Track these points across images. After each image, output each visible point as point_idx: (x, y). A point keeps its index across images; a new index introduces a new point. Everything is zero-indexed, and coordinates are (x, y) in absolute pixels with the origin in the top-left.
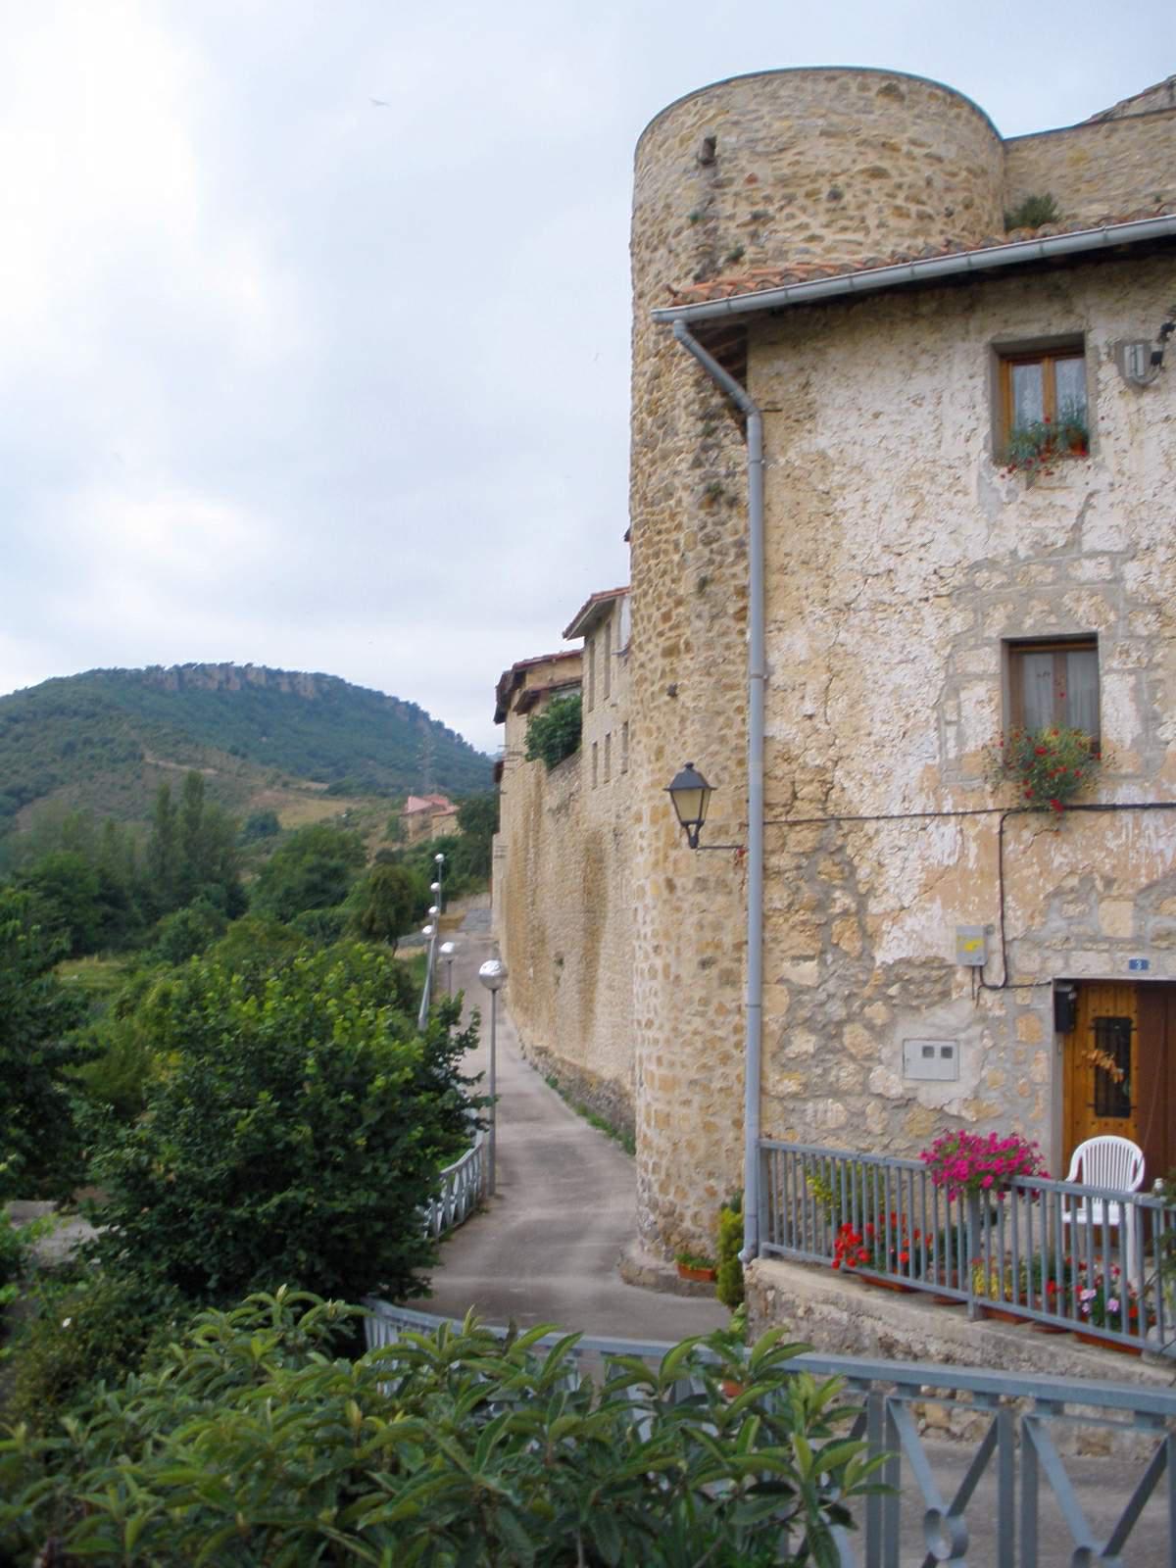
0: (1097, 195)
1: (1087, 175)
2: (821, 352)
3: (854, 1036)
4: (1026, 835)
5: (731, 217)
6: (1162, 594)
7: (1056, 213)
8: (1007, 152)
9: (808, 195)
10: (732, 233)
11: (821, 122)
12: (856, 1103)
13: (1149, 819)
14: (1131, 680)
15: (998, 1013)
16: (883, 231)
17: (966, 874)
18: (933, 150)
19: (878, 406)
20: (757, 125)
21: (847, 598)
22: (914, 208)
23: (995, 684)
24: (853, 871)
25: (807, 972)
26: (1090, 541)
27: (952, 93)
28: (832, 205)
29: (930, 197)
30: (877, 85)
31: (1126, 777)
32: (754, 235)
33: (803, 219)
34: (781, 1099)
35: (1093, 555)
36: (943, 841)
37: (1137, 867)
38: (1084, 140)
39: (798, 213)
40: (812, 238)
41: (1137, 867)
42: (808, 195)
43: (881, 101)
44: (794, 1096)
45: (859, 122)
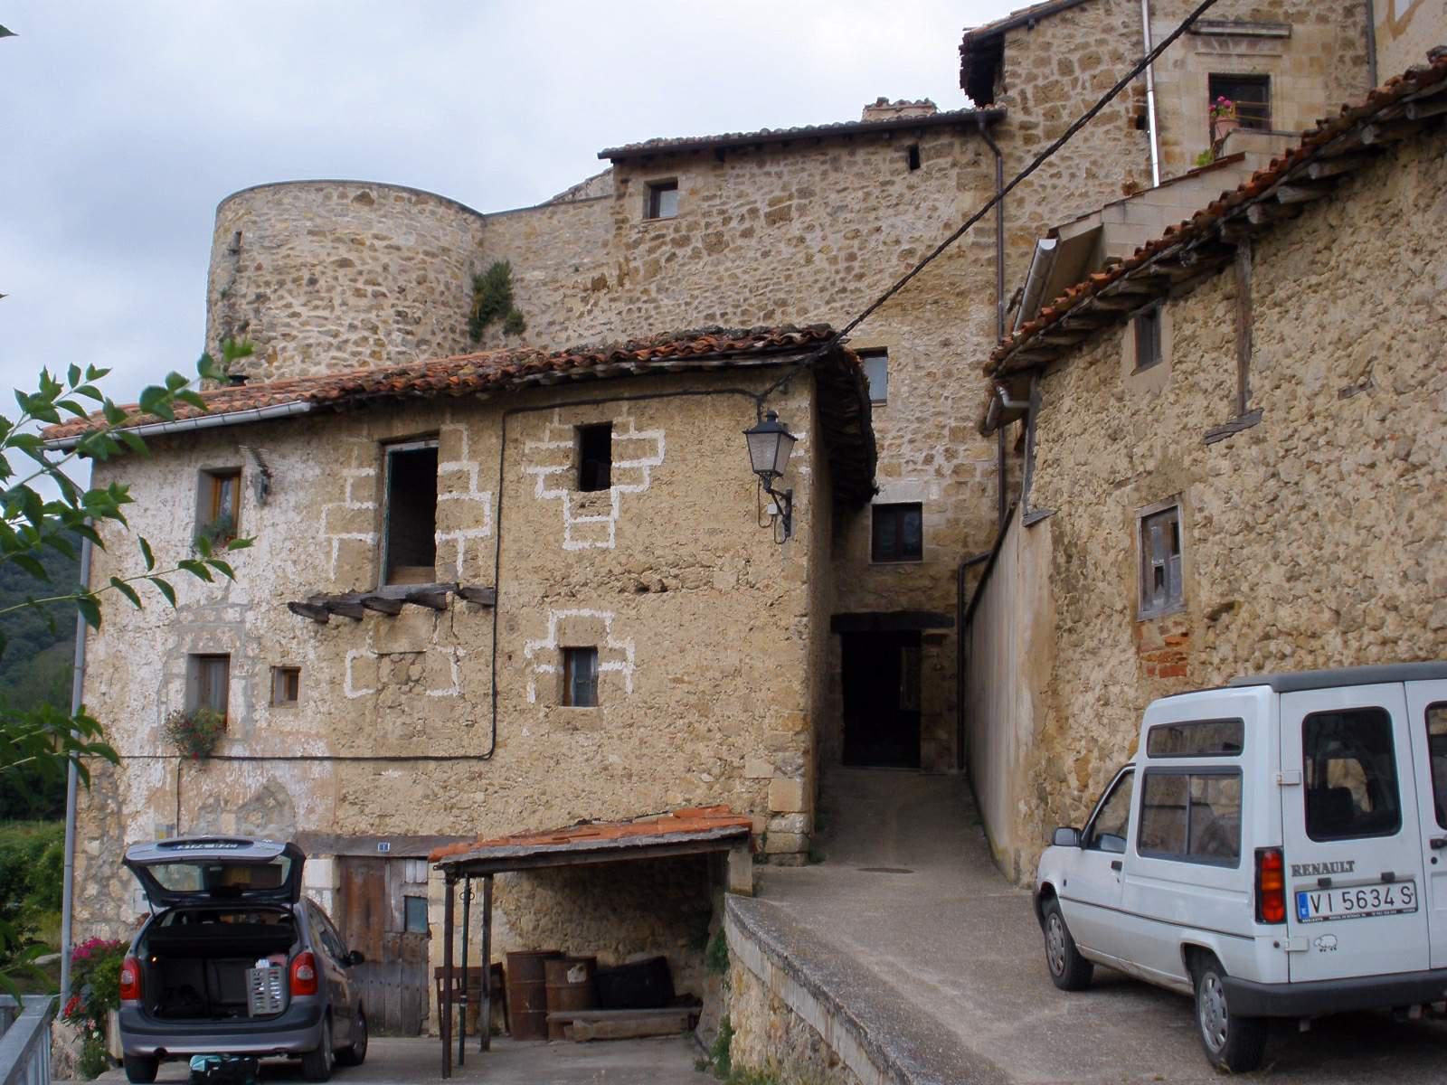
0: (539, 264)
1: (534, 247)
2: (124, 467)
3: (115, 885)
4: (193, 772)
5: (244, 296)
6: (262, 632)
7: (510, 277)
8: (484, 226)
9: (294, 281)
10: (245, 308)
11: (309, 224)
12: (114, 925)
13: (245, 765)
14: (243, 682)
15: (177, 876)
16: (344, 308)
17: (166, 792)
18: (394, 242)
19: (147, 504)
20: (266, 225)
21: (124, 623)
22: (370, 289)
23: (183, 681)
24: (117, 788)
25: (94, 847)
26: (233, 598)
27: (417, 193)
28: (309, 289)
29: (386, 278)
30: (353, 193)
31: (237, 740)
32: (257, 311)
33: (289, 299)
34: (82, 922)
35: (233, 605)
37: (238, 794)
38: (539, 222)
39: (286, 295)
40: (295, 315)
41: (238, 794)
42: (294, 281)
43: (357, 205)
44: (87, 920)
45: (336, 223)
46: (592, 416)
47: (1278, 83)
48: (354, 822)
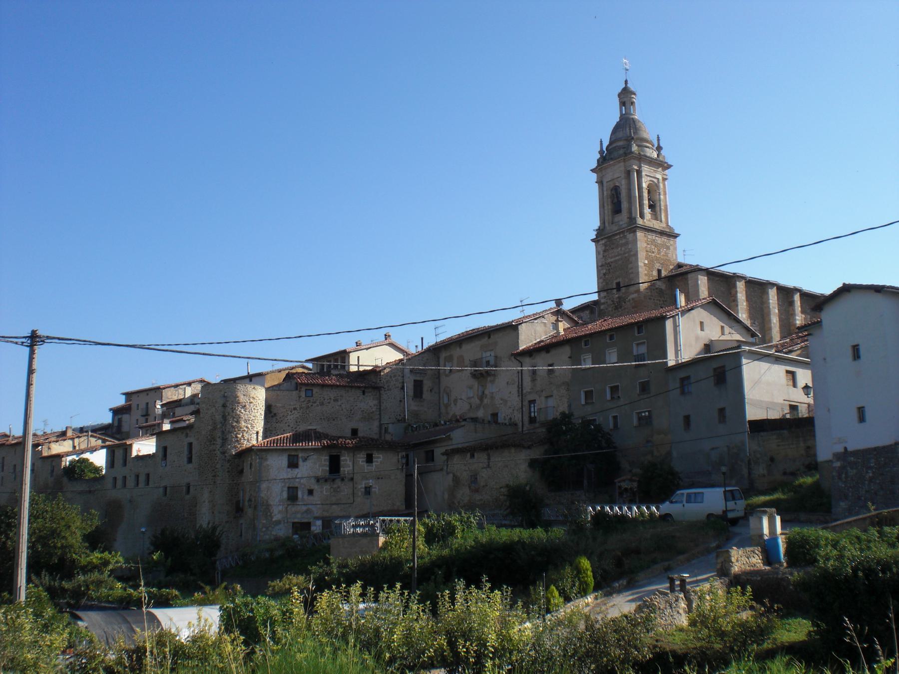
36: (281, 508)
46: (369, 452)
47: (425, 382)
48: (326, 514)
